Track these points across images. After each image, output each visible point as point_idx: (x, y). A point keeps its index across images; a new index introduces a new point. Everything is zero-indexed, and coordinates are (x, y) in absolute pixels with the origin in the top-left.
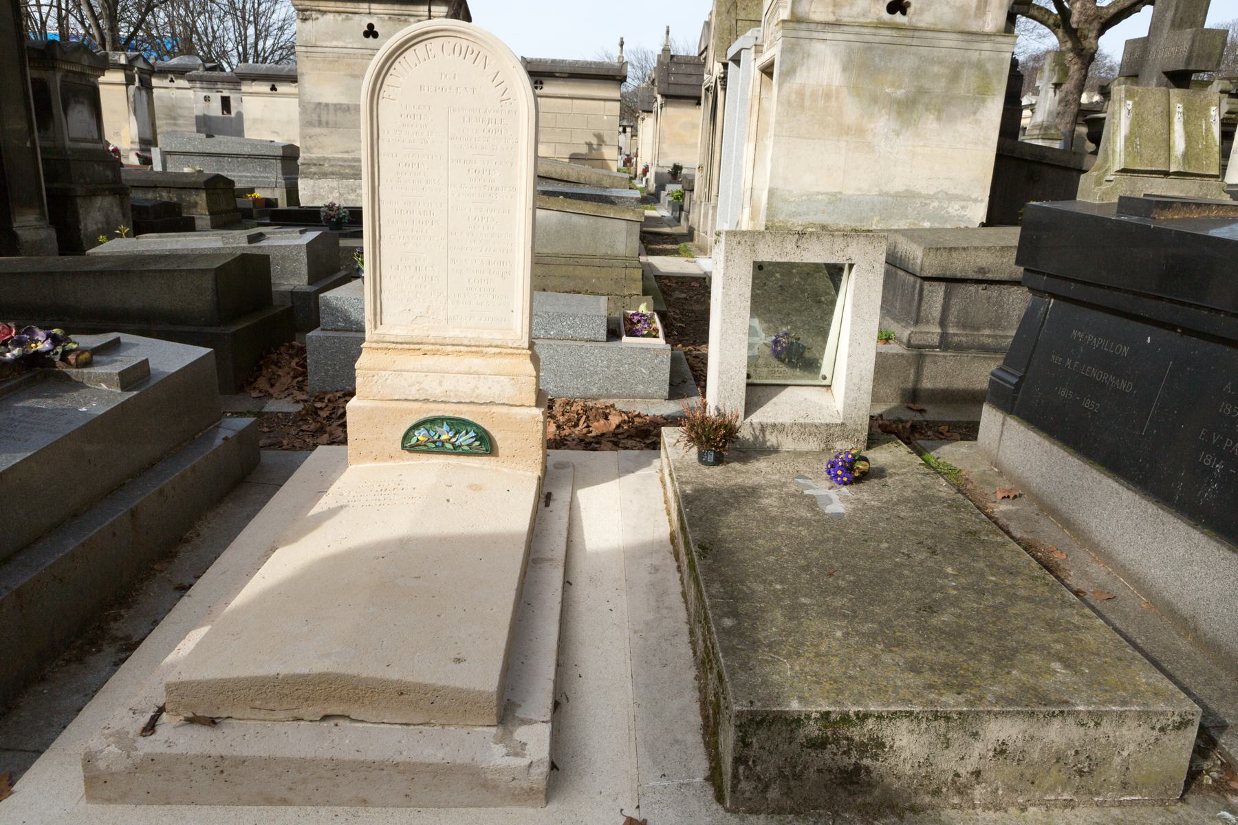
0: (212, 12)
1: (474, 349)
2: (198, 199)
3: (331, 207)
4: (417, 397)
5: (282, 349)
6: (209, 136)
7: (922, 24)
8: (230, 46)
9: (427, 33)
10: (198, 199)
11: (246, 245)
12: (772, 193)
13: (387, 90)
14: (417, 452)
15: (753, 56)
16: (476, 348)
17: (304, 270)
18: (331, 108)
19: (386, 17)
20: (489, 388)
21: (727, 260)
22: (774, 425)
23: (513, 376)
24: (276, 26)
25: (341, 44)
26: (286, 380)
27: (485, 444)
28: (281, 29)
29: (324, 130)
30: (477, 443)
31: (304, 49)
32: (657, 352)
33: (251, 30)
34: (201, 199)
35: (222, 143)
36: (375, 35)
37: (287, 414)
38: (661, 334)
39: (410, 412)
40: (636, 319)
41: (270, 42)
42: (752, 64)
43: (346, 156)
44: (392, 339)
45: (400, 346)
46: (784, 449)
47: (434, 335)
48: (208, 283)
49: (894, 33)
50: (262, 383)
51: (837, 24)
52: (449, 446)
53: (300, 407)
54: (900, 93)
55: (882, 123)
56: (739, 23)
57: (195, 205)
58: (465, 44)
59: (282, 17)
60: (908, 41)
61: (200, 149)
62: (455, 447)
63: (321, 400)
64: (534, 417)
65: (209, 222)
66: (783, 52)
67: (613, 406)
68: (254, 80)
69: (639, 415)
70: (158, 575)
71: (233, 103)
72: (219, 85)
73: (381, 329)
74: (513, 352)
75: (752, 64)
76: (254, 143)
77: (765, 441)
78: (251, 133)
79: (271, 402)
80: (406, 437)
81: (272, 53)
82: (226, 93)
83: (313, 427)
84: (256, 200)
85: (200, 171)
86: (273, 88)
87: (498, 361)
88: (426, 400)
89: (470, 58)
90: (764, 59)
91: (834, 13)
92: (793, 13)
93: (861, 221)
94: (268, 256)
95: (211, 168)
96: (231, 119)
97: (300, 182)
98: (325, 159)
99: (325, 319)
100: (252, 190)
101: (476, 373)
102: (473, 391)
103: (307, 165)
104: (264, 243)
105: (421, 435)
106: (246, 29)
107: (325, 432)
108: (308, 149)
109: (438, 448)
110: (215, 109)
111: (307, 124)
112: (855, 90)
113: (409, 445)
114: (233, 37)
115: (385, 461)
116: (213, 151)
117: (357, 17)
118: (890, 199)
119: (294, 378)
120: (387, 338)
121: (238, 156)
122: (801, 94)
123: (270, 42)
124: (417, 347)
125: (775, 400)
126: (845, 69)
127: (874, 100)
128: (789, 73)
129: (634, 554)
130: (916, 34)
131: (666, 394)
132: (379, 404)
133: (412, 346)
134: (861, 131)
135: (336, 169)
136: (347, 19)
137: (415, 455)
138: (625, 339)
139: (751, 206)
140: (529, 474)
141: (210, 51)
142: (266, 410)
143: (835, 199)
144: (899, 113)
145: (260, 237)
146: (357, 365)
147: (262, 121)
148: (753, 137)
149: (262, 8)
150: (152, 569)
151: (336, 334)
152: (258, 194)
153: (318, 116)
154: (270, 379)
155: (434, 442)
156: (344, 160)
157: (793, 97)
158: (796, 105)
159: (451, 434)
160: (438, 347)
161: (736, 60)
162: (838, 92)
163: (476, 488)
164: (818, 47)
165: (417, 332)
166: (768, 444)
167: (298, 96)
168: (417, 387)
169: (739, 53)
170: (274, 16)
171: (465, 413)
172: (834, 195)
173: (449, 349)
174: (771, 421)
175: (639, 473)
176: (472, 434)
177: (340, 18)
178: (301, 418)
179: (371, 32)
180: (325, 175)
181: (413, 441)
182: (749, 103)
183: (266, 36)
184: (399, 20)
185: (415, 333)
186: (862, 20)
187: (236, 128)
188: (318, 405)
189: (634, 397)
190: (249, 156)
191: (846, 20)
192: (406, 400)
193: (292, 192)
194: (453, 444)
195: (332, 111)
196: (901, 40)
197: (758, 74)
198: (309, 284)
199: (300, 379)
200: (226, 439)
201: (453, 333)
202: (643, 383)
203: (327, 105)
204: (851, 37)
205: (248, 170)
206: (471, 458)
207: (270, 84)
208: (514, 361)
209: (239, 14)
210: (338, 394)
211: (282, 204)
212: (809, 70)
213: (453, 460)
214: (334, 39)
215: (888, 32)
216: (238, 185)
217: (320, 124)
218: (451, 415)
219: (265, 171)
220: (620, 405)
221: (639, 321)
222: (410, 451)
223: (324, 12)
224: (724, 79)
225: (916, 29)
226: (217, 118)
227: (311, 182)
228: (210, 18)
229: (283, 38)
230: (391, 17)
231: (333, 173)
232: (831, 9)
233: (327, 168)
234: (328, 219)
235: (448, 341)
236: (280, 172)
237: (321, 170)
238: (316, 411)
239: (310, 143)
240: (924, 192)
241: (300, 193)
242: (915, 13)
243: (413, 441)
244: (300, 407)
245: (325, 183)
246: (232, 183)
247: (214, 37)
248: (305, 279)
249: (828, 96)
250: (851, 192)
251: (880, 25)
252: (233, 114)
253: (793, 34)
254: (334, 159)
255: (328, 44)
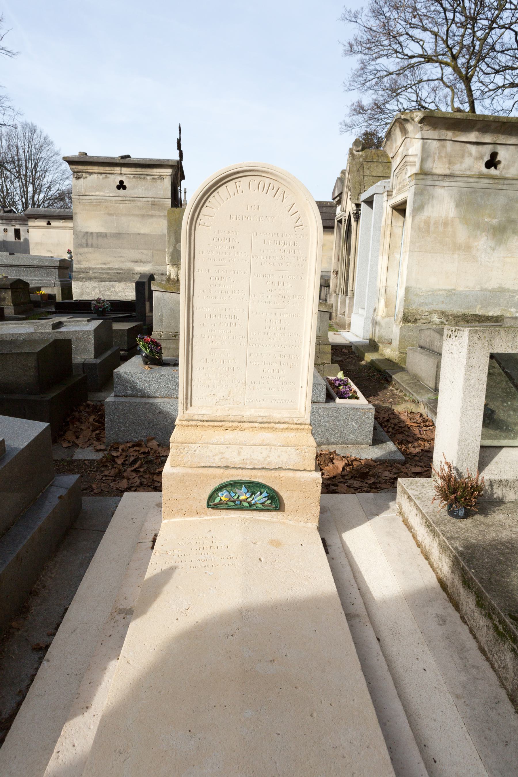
0: (7, 177)
1: (266, 425)
2: (6, 295)
3: (99, 301)
4: (220, 464)
5: (82, 408)
6: (12, 254)
7: (508, 176)
8: (17, 198)
9: (250, 171)
10: (6, 295)
11: (51, 331)
12: (407, 290)
13: (203, 219)
14: (217, 508)
15: (385, 198)
16: (268, 425)
17: (92, 348)
18: (95, 235)
19: (132, 176)
20: (275, 458)
21: (469, 352)
22: (500, 481)
23: (298, 447)
24: (46, 186)
25: (102, 194)
26: (87, 433)
27: (275, 502)
28: (49, 188)
29: (90, 250)
30: (269, 502)
31: (77, 197)
32: (364, 411)
33: (30, 189)
34: (8, 295)
35: (18, 259)
36: (124, 188)
37: (92, 461)
38: (359, 394)
39: (215, 477)
40: (337, 383)
41: (42, 196)
42: (384, 206)
43: (104, 266)
44: (200, 418)
45: (206, 424)
46: (507, 500)
47: (234, 414)
48: (32, 363)
49: (491, 181)
50: (70, 436)
51: (451, 176)
52: (246, 504)
53: (101, 455)
54: (495, 222)
55: (483, 242)
56: (366, 178)
57: (4, 299)
58: (267, 181)
59: (50, 180)
60: (500, 187)
61: (6, 262)
62: (250, 505)
63: (116, 449)
64: (314, 480)
65: (13, 311)
66: (415, 194)
67: (335, 452)
68: (36, 218)
69: (355, 460)
70: (17, 633)
71: (22, 233)
72: (13, 222)
73: (191, 410)
74: (297, 427)
75: (384, 206)
76: (35, 257)
77: (493, 494)
78: (34, 251)
79: (78, 450)
80: (211, 497)
81: (43, 202)
82: (17, 227)
83: (113, 472)
84: (43, 296)
85: (6, 277)
86: (49, 223)
87: (285, 434)
88: (227, 467)
89: (271, 192)
90: (397, 199)
91: (449, 168)
92: (421, 168)
93: (469, 308)
94: (69, 341)
95: (13, 275)
96: (20, 243)
97: (73, 283)
98: (90, 268)
99: (118, 387)
100: (39, 289)
101: (269, 445)
102: (265, 459)
103: (79, 272)
104: (62, 329)
105: (223, 496)
106: (27, 188)
107: (123, 478)
108: (79, 262)
109: (238, 506)
110: (11, 236)
111: (78, 245)
112: (465, 220)
113: (213, 503)
114: (19, 193)
115: (192, 516)
116: (13, 264)
117: (112, 176)
118: (488, 293)
119: (93, 431)
120: (196, 417)
121: (30, 266)
122: (427, 223)
123: (42, 196)
124: (220, 424)
125: (496, 459)
126: (457, 206)
127: (477, 226)
128: (418, 209)
129: (416, 600)
130: (506, 182)
131: (370, 441)
132: (190, 471)
133: (216, 424)
134: (468, 248)
135: (97, 275)
136: (106, 177)
137: (217, 511)
138: (338, 400)
139: (386, 298)
140: (309, 525)
141: (5, 201)
142: (75, 458)
143: (451, 293)
144: (494, 235)
145: (59, 325)
146: (171, 440)
147: (41, 244)
148: (387, 251)
149: (38, 174)
150: (11, 627)
151: (127, 400)
152: (44, 291)
153: (85, 240)
154: (75, 432)
155: (234, 501)
156: (103, 269)
157: (422, 225)
158: (424, 230)
159: (248, 495)
160: (238, 424)
161: (369, 202)
162: (452, 221)
163: (276, 543)
164: (439, 191)
165: (219, 412)
166: (495, 496)
167: (73, 228)
168: (220, 456)
169: (372, 196)
170: (45, 180)
171: (259, 477)
172: (450, 291)
173: (246, 425)
174: (498, 478)
175: (382, 515)
176: (265, 494)
177: (101, 177)
178: (102, 464)
179: (121, 186)
180: (90, 279)
181: (217, 500)
182: (382, 229)
183: (39, 193)
184: (140, 178)
185: (219, 413)
186: (468, 173)
187: (25, 247)
188: (115, 454)
189: (347, 444)
190: (38, 267)
191: (457, 173)
192: (210, 467)
193: (67, 290)
194: (249, 503)
195: (95, 237)
196: (495, 186)
197: (390, 210)
198: (96, 357)
199: (98, 432)
200: (60, 497)
201: (249, 413)
202: (354, 433)
203: (92, 233)
204: (462, 184)
205: (36, 276)
206: (262, 513)
207: (47, 221)
208: (298, 434)
209: (22, 177)
210: (129, 445)
211: (59, 299)
212: (433, 207)
213: (248, 515)
214: (97, 190)
215: (487, 181)
216: (31, 286)
217: (87, 245)
218: (248, 479)
219: (47, 276)
220: (340, 450)
221: (340, 385)
222: (213, 508)
223: (91, 173)
224: (357, 216)
225: (506, 179)
226: (11, 242)
227: (81, 284)
228: (5, 181)
229: (51, 193)
230: (135, 176)
231: (95, 278)
232: (447, 166)
233: (91, 274)
234: (97, 309)
235: (245, 419)
236: (57, 277)
237: (87, 276)
238: (113, 459)
239: (80, 258)
240: (511, 288)
241: (73, 291)
242: (504, 168)
243: (217, 500)
244: (101, 455)
245: (90, 284)
246: (28, 284)
247: (7, 193)
248: (92, 355)
249: (446, 224)
250: (461, 289)
251: (481, 176)
252: (22, 240)
253: (423, 182)
254: (96, 268)
255: (93, 194)
